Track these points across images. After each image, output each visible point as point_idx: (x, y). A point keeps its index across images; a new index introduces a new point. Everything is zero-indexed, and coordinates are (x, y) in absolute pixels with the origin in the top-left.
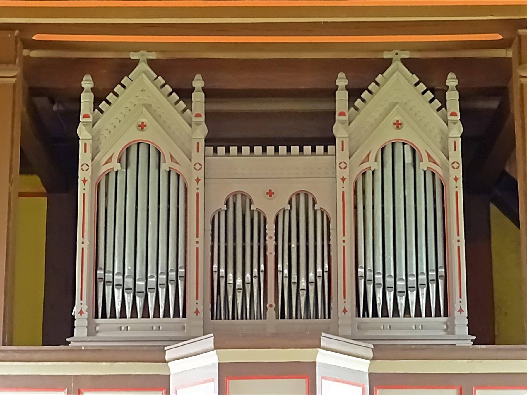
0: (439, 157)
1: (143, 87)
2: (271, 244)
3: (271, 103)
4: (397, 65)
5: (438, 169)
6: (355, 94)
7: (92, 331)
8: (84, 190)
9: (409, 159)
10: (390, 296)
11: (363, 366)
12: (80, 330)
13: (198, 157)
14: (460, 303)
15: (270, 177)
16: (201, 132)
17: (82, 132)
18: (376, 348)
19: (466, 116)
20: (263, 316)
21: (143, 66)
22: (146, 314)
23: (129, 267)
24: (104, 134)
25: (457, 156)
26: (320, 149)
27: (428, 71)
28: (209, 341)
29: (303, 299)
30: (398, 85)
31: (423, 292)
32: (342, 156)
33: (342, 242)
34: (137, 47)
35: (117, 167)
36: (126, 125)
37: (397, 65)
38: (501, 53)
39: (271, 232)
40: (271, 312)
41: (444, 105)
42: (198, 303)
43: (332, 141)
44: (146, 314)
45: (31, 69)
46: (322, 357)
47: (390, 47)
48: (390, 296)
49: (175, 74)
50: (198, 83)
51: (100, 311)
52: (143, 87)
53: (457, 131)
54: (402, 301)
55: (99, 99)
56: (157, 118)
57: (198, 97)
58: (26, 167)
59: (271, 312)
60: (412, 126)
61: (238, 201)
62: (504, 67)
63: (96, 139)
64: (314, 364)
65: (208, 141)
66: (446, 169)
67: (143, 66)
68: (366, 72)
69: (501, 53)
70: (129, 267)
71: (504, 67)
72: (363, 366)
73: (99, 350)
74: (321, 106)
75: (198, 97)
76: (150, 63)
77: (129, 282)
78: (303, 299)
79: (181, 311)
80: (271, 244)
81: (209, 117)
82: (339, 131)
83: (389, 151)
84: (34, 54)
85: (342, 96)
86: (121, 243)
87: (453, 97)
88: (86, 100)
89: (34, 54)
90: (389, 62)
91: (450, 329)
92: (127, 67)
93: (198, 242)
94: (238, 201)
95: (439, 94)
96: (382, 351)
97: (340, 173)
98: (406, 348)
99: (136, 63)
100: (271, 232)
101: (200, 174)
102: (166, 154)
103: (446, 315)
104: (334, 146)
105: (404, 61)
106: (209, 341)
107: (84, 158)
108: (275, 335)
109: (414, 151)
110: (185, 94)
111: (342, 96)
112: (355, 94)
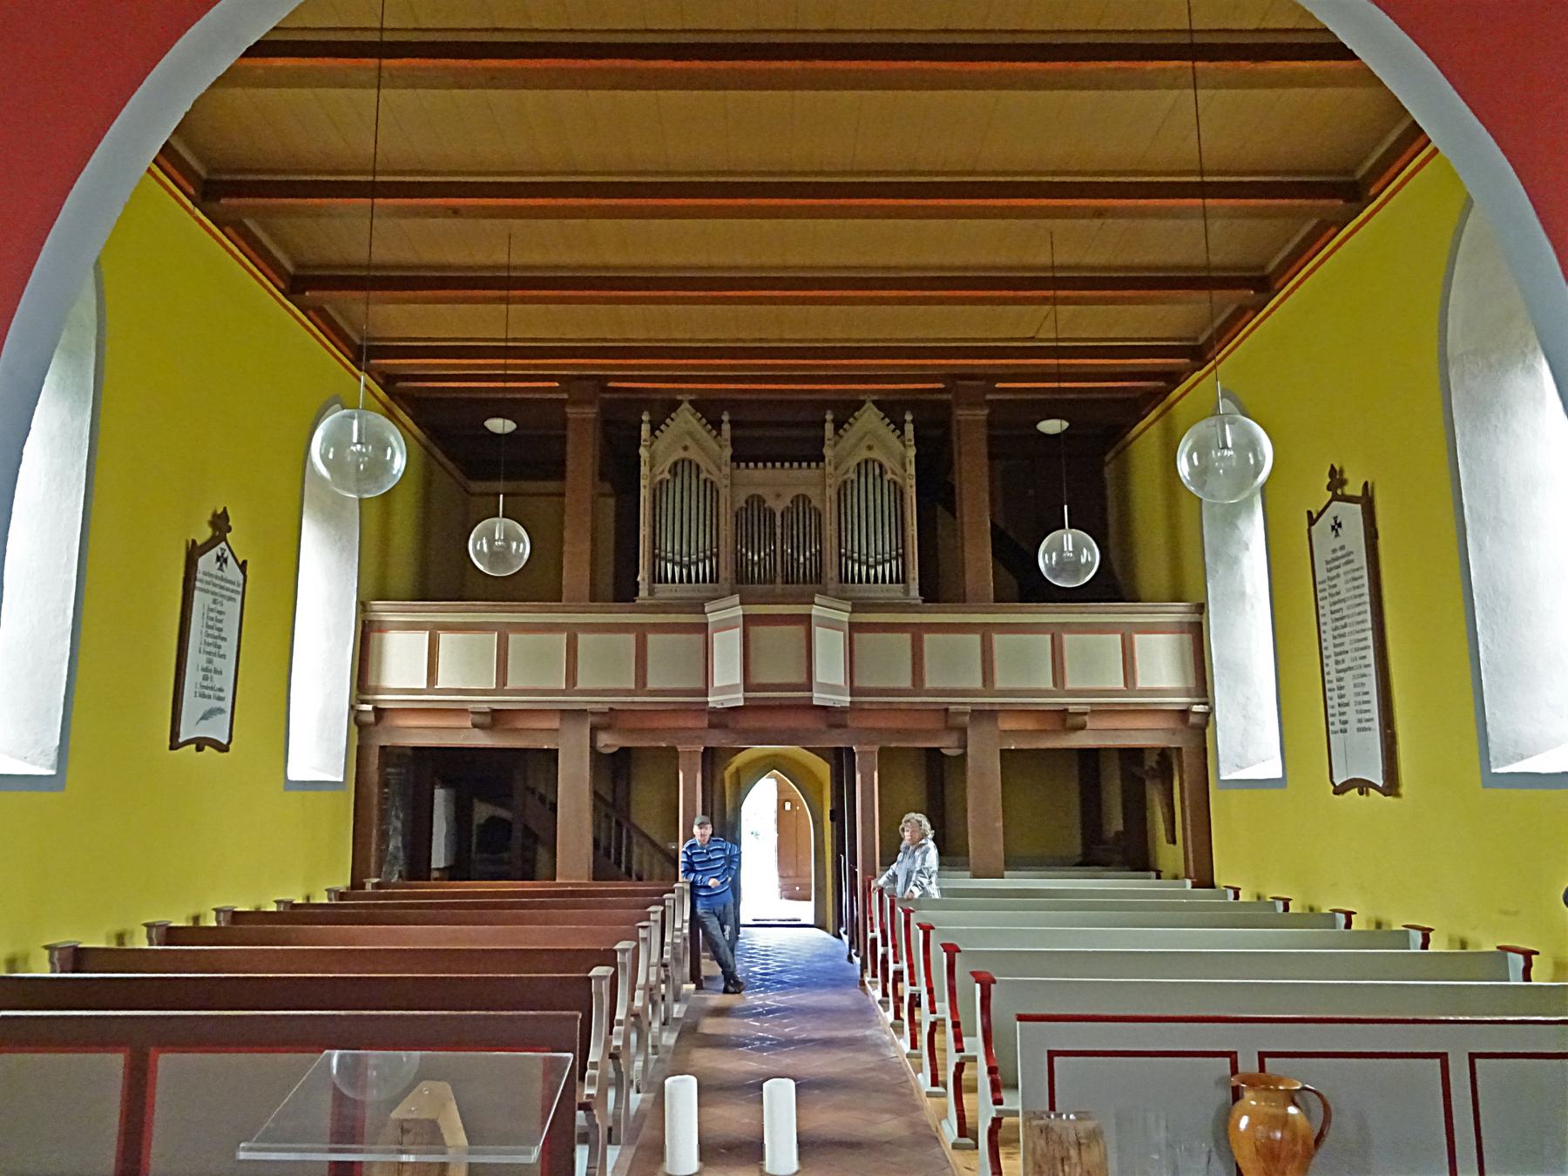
0: (899, 470)
1: (686, 419)
2: (778, 531)
3: (776, 428)
4: (869, 405)
5: (898, 480)
6: (838, 425)
7: (651, 592)
8: (645, 493)
9: (877, 471)
10: (864, 569)
11: (845, 617)
12: (643, 592)
13: (726, 470)
14: (914, 573)
15: (778, 484)
16: (728, 452)
17: (642, 451)
18: (853, 606)
19: (919, 441)
20: (773, 581)
21: (686, 405)
22: (689, 581)
23: (677, 547)
24: (657, 455)
25: (912, 470)
26: (813, 465)
27: (891, 409)
28: (736, 598)
29: (871, 519)
30: (869, 419)
31: (880, 569)
32: (830, 469)
33: (830, 530)
34: (681, 391)
35: (667, 476)
36: (672, 445)
37: (869, 405)
38: (945, 397)
39: (778, 523)
40: (779, 580)
41: (903, 432)
42: (726, 573)
43: (822, 458)
44: (689, 581)
45: (606, 407)
46: (815, 611)
47: (865, 392)
48: (864, 569)
49: (709, 409)
50: (726, 417)
51: (657, 578)
52: (686, 419)
53: (912, 453)
54: (872, 572)
55: (654, 428)
56: (697, 441)
57: (726, 428)
58: (603, 476)
59: (779, 580)
60: (880, 447)
61: (756, 501)
62: (947, 407)
63: (652, 457)
64: (810, 616)
65: (733, 458)
66: (904, 479)
67: (686, 405)
68: (847, 409)
69: (945, 397)
70: (677, 547)
71: (947, 407)
72: (845, 617)
73: (658, 606)
74: (811, 433)
75: (726, 428)
76: (691, 402)
77: (677, 558)
78: (871, 519)
79: (714, 579)
80: (778, 531)
81: (734, 441)
82: (828, 452)
83: (863, 466)
84: (607, 396)
85: (829, 427)
86: (672, 534)
87: (909, 428)
88: (645, 429)
89: (607, 396)
90: (863, 402)
91: (907, 592)
92: (675, 405)
93: (726, 530)
94: (756, 501)
95: (900, 426)
96: (858, 606)
97: (828, 481)
98: (873, 605)
99: (681, 402)
100: (778, 523)
101: (728, 482)
102: (703, 467)
103: (904, 581)
104: (702, 636)
105: (874, 402)
106: (736, 598)
107: (644, 470)
108: (783, 595)
109: (881, 466)
110: (716, 425)
111: (829, 427)
112: (838, 425)
